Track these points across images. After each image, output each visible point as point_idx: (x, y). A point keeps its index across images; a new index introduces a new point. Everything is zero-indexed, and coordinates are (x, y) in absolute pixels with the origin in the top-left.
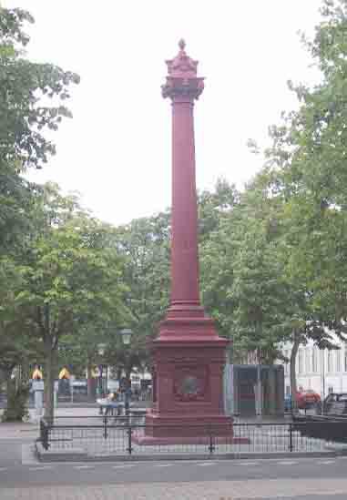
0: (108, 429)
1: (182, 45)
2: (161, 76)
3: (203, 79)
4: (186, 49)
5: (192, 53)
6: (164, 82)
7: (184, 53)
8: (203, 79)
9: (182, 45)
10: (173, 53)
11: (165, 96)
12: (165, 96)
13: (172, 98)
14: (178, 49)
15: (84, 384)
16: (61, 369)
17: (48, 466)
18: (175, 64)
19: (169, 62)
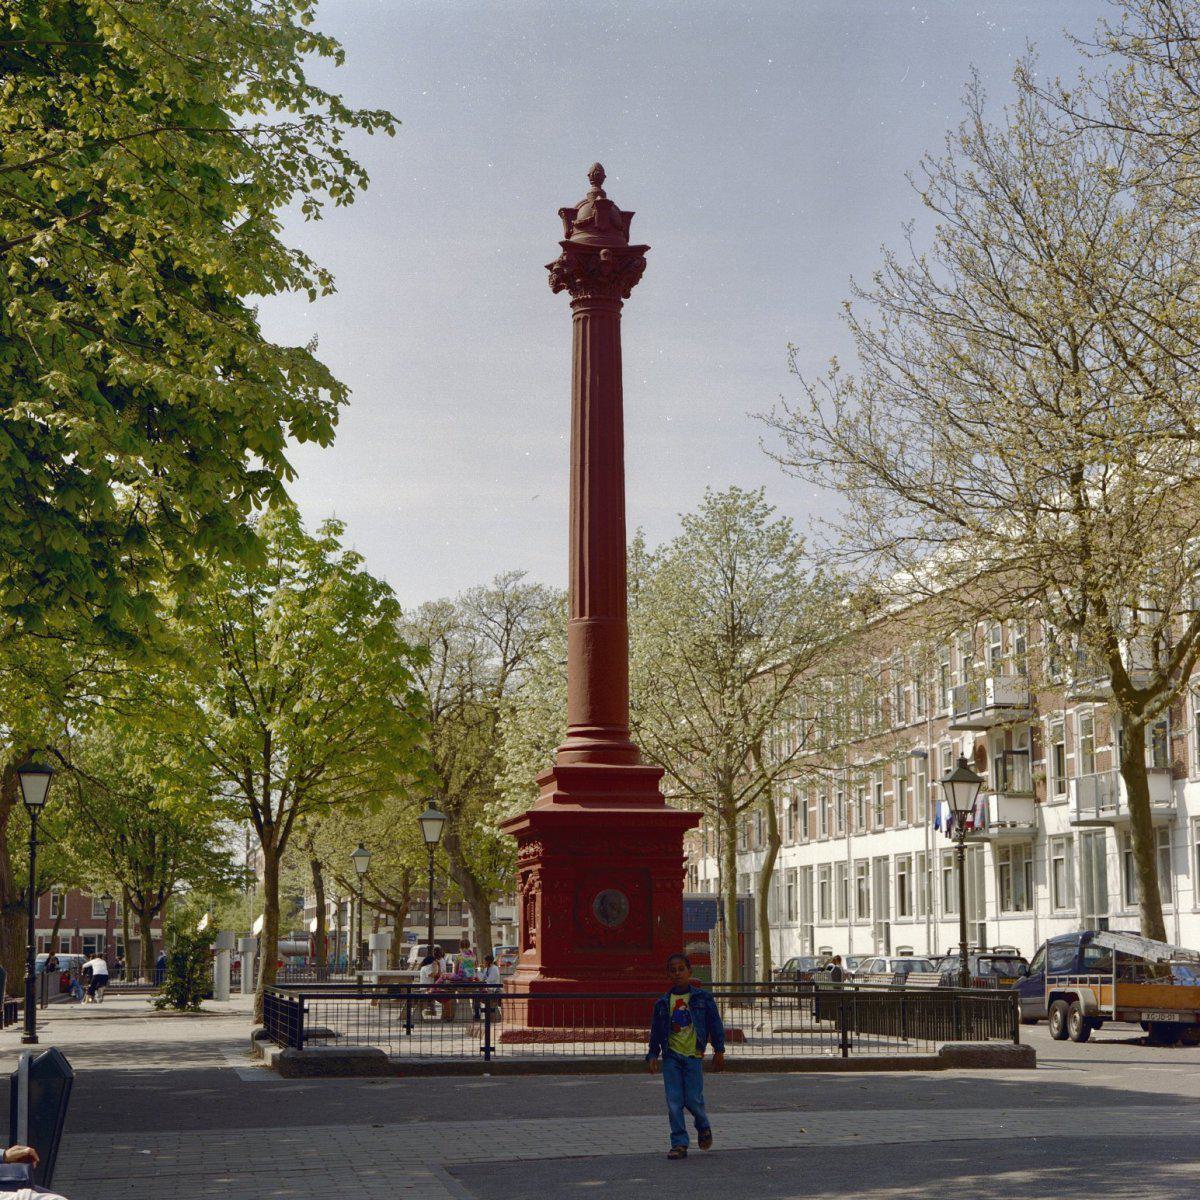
0: (1181, 295)
1: (598, 176)
2: (549, 243)
3: (645, 248)
4: (604, 187)
5: (617, 193)
6: (556, 254)
7: (603, 194)
8: (645, 248)
9: (598, 176)
10: (578, 193)
11: (556, 290)
12: (556, 290)
13: (573, 291)
14: (590, 188)
15: (53, 887)
16: (669, 997)
17: (302, 1085)
18: (581, 215)
19: (568, 214)
